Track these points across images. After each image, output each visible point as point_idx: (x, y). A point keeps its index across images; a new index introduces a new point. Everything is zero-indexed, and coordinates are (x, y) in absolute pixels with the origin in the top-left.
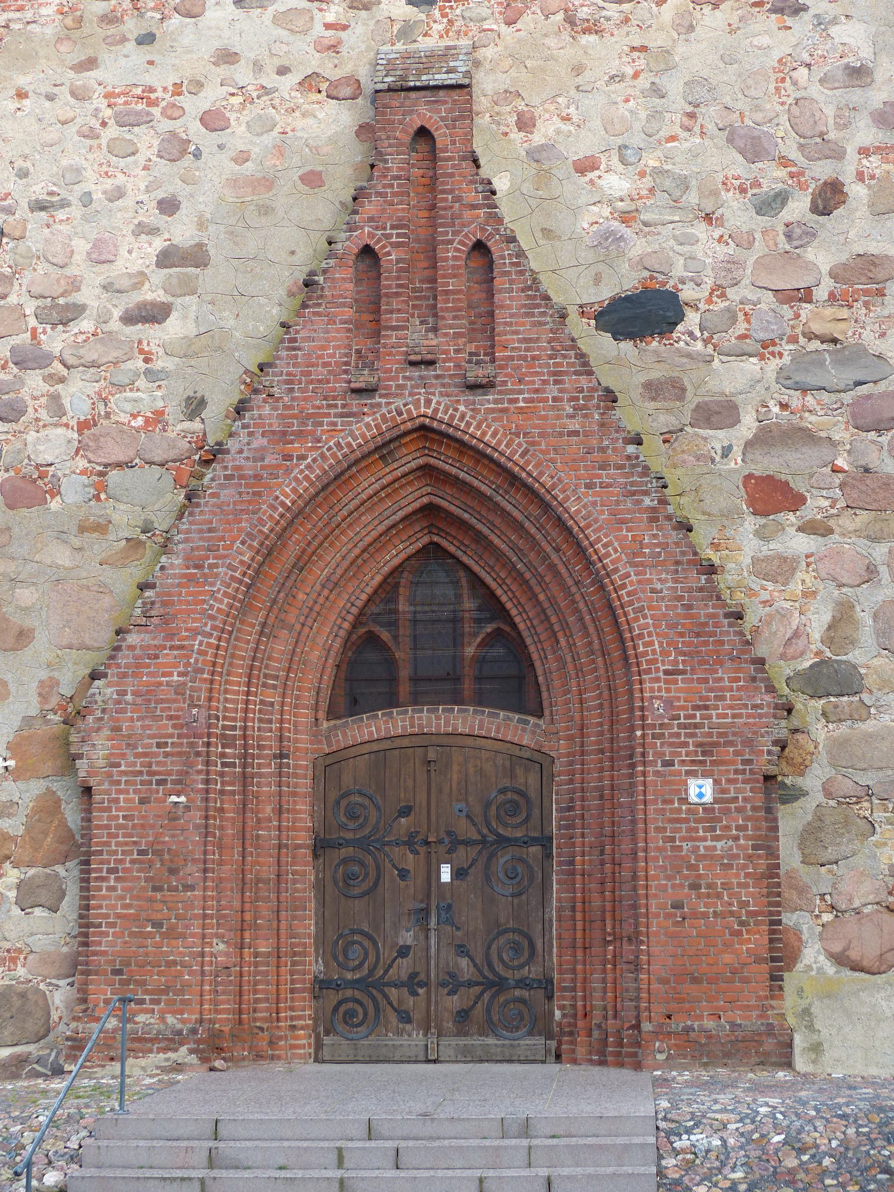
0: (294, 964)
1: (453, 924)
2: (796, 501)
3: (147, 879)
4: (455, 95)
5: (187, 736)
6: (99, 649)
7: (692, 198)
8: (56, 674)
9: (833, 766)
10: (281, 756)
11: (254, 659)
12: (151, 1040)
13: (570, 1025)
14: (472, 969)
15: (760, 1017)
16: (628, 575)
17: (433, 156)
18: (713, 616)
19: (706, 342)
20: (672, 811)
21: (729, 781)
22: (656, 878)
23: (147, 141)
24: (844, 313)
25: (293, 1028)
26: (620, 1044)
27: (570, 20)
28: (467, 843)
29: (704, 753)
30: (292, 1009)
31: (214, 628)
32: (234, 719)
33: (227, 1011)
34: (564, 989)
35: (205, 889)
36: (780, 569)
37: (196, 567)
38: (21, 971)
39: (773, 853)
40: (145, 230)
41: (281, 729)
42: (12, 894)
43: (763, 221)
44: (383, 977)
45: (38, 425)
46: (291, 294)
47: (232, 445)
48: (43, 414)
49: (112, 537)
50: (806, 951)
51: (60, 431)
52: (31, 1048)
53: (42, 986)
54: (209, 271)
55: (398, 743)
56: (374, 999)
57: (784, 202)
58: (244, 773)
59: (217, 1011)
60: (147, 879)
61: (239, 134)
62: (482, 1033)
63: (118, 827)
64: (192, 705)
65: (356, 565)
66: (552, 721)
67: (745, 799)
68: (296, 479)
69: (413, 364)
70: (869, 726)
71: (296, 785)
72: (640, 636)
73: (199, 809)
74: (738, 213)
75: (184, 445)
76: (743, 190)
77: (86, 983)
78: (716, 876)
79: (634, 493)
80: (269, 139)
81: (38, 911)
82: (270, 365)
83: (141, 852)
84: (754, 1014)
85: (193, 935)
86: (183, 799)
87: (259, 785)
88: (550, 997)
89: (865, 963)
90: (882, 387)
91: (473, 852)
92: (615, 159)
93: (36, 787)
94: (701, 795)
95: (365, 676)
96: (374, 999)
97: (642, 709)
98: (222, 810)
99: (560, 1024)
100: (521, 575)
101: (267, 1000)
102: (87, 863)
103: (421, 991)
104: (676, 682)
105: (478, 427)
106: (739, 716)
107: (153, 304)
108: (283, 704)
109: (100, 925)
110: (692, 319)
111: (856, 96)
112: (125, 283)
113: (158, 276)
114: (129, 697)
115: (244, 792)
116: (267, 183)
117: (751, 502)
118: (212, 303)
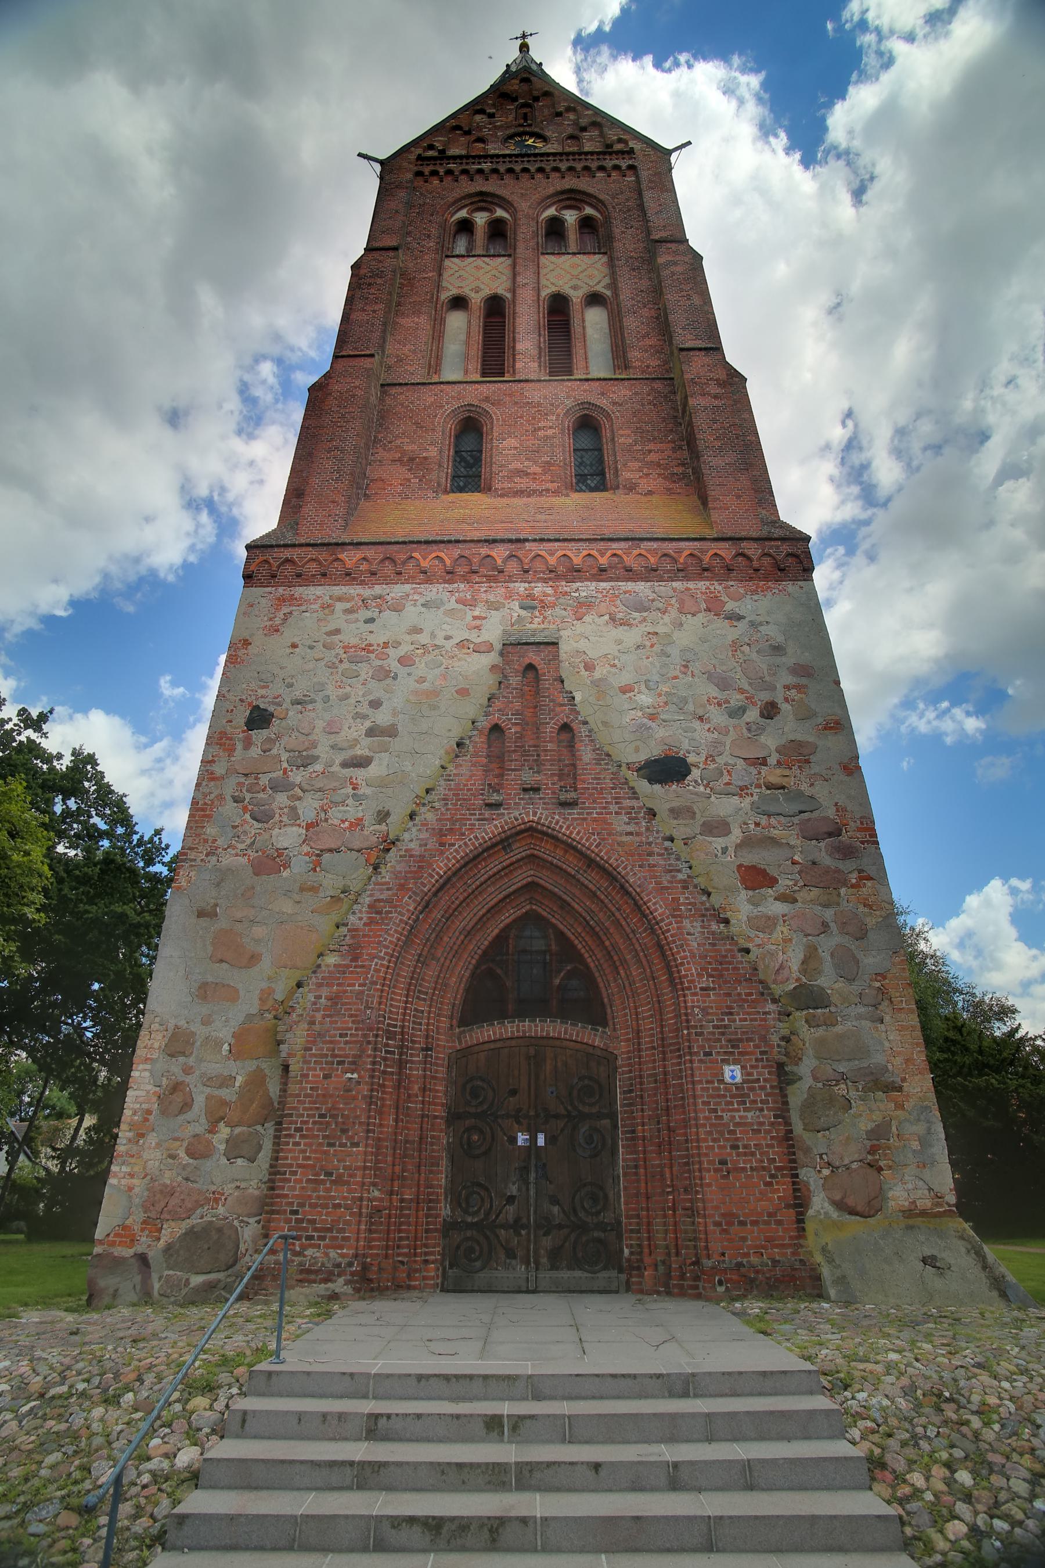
0: (429, 1208)
1: (547, 1179)
2: (772, 882)
3: (324, 1137)
4: (550, 648)
5: (362, 1029)
6: (305, 969)
7: (690, 707)
8: (273, 985)
9: (818, 1058)
10: (427, 1049)
11: (412, 978)
12: (316, 1272)
13: (638, 1261)
14: (562, 1215)
15: (793, 1254)
16: (671, 923)
17: (537, 679)
18: (731, 950)
19: (706, 786)
20: (714, 1089)
21: (752, 1067)
22: (706, 1140)
23: (365, 670)
24: (787, 772)
25: (426, 1262)
26: (682, 1277)
27: (613, 619)
28: (557, 1116)
29: (733, 1047)
30: (426, 1246)
31: (386, 953)
32: (396, 1020)
33: (377, 1247)
34: (632, 1231)
35: (366, 1146)
36: (767, 924)
37: (377, 913)
38: (221, 1210)
39: (788, 1123)
40: (358, 716)
41: (427, 1030)
42: (222, 1147)
43: (735, 721)
44: (494, 1221)
45: (281, 825)
46: (447, 753)
47: (406, 836)
48: (285, 819)
49: (322, 895)
50: (814, 1199)
51: (295, 829)
52: (221, 1276)
53: (236, 1223)
54: (397, 739)
55: (508, 1043)
56: (487, 1238)
57: (744, 712)
58: (400, 1059)
59: (371, 1248)
60: (324, 1137)
61: (420, 668)
62: (570, 1268)
63: (306, 1096)
64: (367, 1007)
65: (482, 922)
66: (615, 1029)
67: (765, 1080)
68: (448, 858)
69: (525, 790)
70: (839, 1029)
71: (436, 1071)
72: (682, 964)
73: (366, 1083)
74: (718, 717)
75: (374, 839)
76: (719, 705)
77: (269, 1221)
78: (749, 1139)
79: (671, 871)
80: (437, 671)
81: (239, 1161)
82: (432, 789)
83: (322, 1116)
84: (789, 1251)
85: (355, 1183)
86: (355, 1076)
87: (411, 1069)
88: (620, 1237)
89: (859, 1209)
90: (816, 814)
91: (561, 1123)
92: (643, 687)
93: (251, 1065)
94: (733, 1077)
95: (483, 1000)
96: (487, 1238)
97: (686, 1015)
98: (383, 1086)
99: (629, 1260)
100: (593, 929)
101: (408, 1238)
102: (280, 1123)
103: (523, 1232)
104: (709, 996)
105: (568, 828)
106: (755, 1020)
107: (361, 757)
108: (429, 1012)
109: (285, 1173)
110: (695, 773)
111: (779, 660)
112: (345, 745)
113: (366, 741)
114: (323, 1000)
115: (400, 1073)
116: (435, 693)
117: (743, 881)
118: (398, 756)
